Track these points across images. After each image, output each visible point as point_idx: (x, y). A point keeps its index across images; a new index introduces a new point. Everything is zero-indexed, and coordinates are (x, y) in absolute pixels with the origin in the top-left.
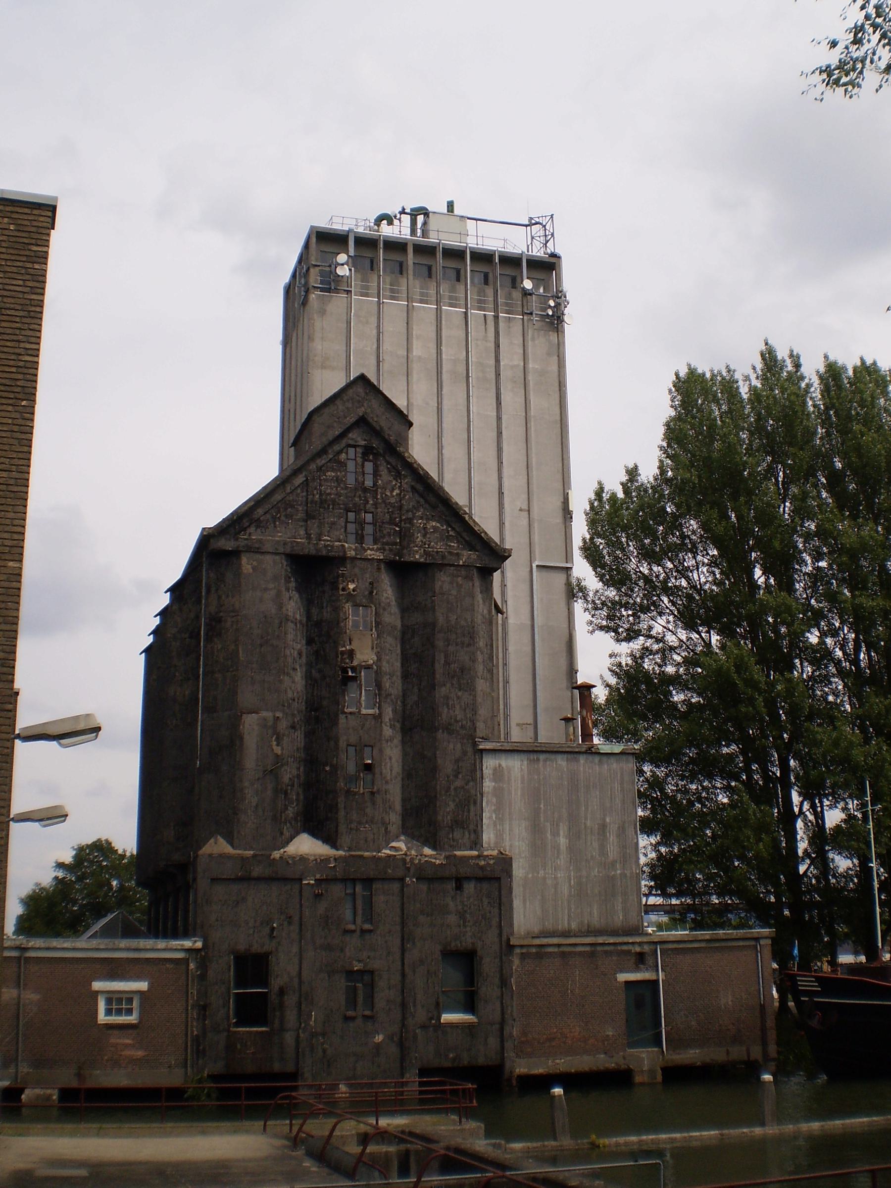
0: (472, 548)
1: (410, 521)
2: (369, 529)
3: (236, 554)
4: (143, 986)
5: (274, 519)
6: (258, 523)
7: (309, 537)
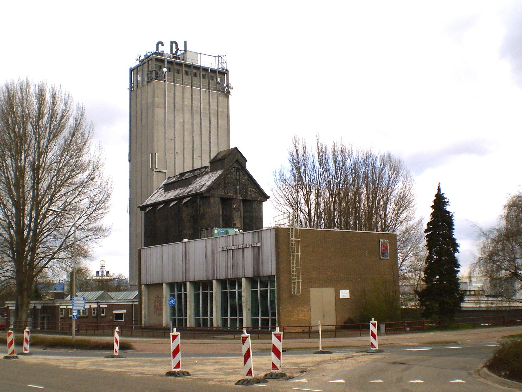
0: (261, 196)
1: (247, 188)
2: (238, 191)
3: (209, 197)
4: (125, 311)
5: (217, 188)
6: (214, 189)
7: (225, 193)
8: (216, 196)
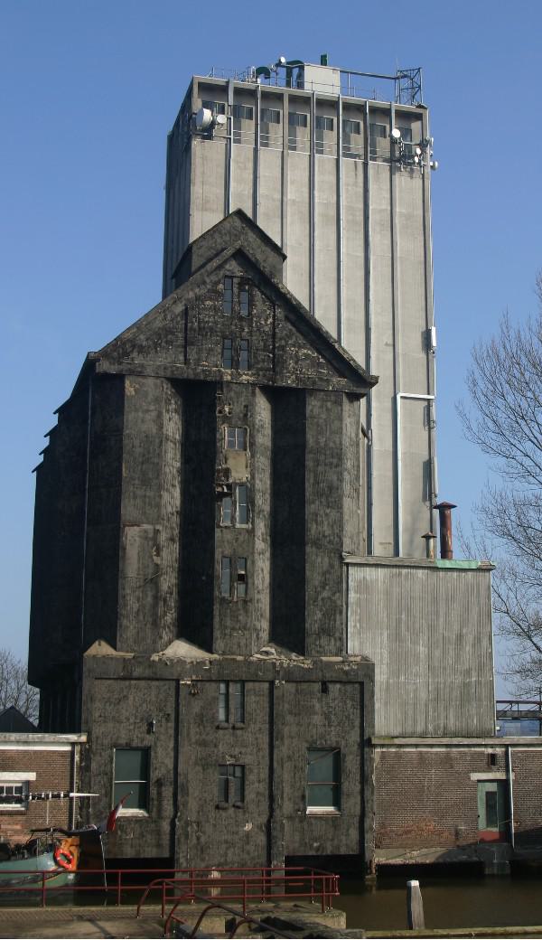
1: (283, 348)
7: (186, 361)
8: (149, 371)
